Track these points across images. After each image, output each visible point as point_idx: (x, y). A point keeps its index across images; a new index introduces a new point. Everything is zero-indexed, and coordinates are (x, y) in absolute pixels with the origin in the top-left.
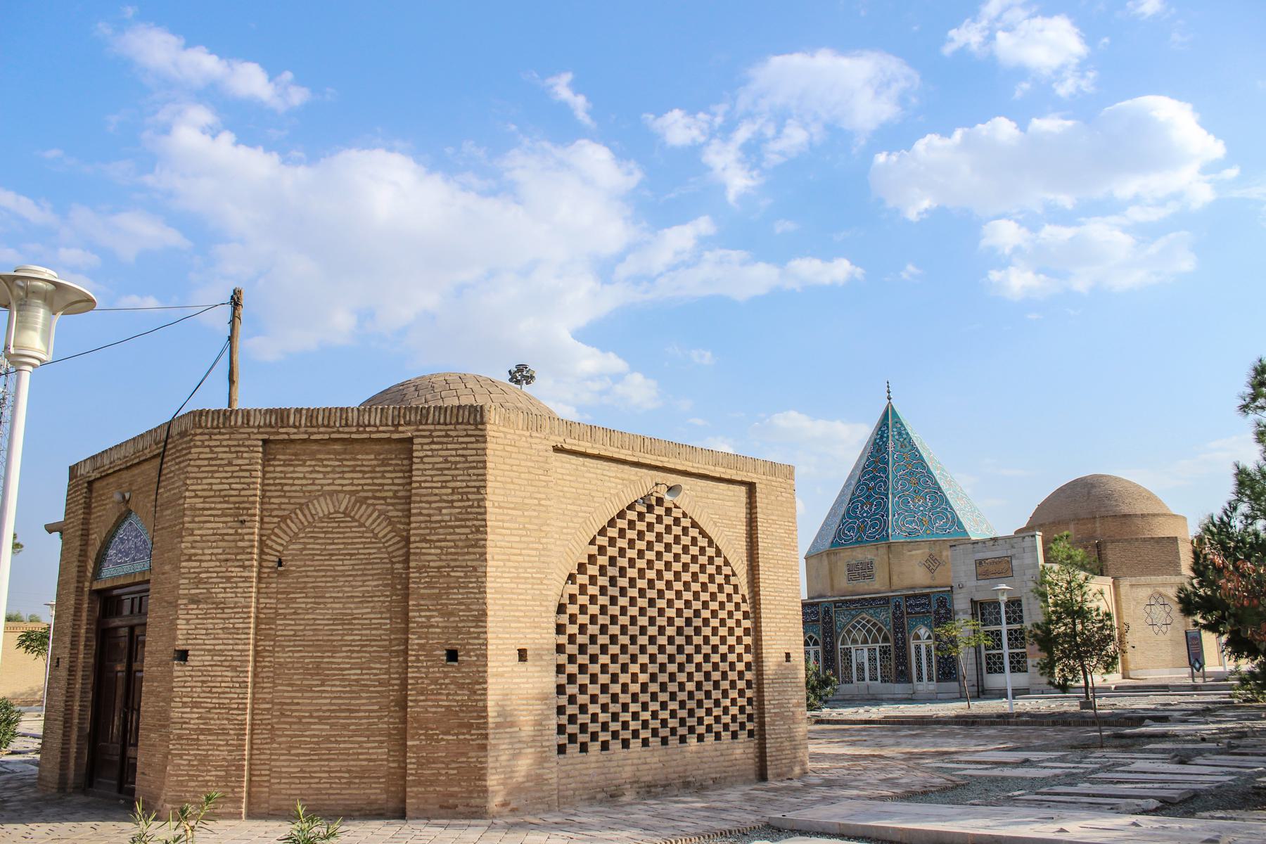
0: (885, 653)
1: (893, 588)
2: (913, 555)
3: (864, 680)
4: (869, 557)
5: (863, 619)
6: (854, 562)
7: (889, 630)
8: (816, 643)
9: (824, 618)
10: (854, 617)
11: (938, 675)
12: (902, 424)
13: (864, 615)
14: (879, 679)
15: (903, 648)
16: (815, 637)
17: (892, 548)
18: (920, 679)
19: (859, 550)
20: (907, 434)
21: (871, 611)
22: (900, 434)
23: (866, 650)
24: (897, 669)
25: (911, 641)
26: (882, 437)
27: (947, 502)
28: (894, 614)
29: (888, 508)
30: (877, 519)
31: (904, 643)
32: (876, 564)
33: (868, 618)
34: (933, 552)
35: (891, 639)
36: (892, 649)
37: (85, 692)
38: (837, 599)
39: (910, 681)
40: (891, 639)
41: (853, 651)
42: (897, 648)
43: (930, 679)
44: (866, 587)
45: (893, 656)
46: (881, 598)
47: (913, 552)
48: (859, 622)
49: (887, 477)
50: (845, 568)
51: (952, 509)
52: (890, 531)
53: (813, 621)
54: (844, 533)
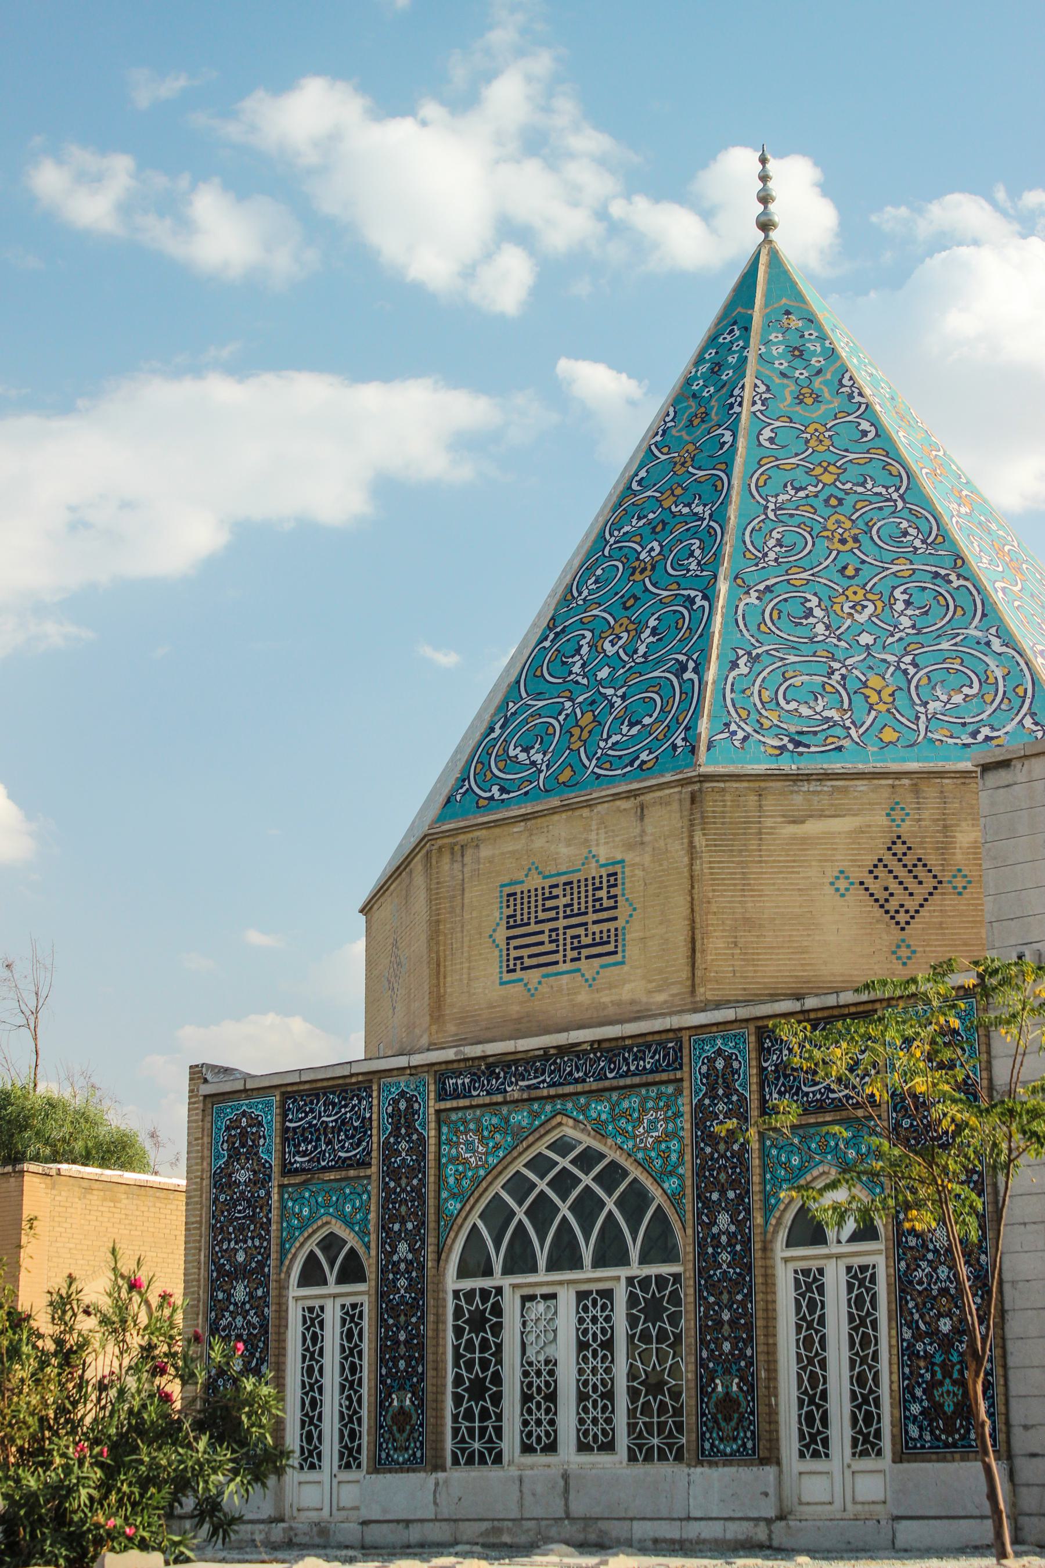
0: (654, 1310)
1: (705, 992)
2: (804, 841)
3: (551, 1448)
4: (603, 853)
5: (562, 1147)
6: (536, 882)
7: (675, 1199)
8: (352, 1272)
9: (389, 1151)
10: (521, 1136)
11: (904, 1421)
12: (811, 320)
13: (569, 1131)
14: (622, 1441)
15: (738, 1283)
16: (351, 1240)
17: (710, 805)
18: (311, 1458)
19: (560, 825)
20: (832, 354)
21: (600, 1109)
22: (798, 353)
23: (567, 1300)
24: (703, 1391)
25: (780, 1250)
26: (717, 368)
27: (988, 612)
28: (702, 1116)
29: (706, 635)
30: (657, 685)
31: (744, 1263)
32: (632, 887)
33: (588, 1141)
34: (906, 828)
35: (684, 1239)
36: (688, 1293)
37: (770, 1432)
38: (450, 1054)
39: (770, 1457)
40: (684, 1239)
41: (511, 1304)
42: (712, 1287)
43: (349, 1458)
44: (583, 997)
45: (688, 1324)
46: (644, 1043)
47: (812, 827)
48: (541, 1165)
49: (719, 517)
50: (495, 914)
51: (1009, 641)
52: (703, 726)
53: (344, 1164)
54: (508, 762)
